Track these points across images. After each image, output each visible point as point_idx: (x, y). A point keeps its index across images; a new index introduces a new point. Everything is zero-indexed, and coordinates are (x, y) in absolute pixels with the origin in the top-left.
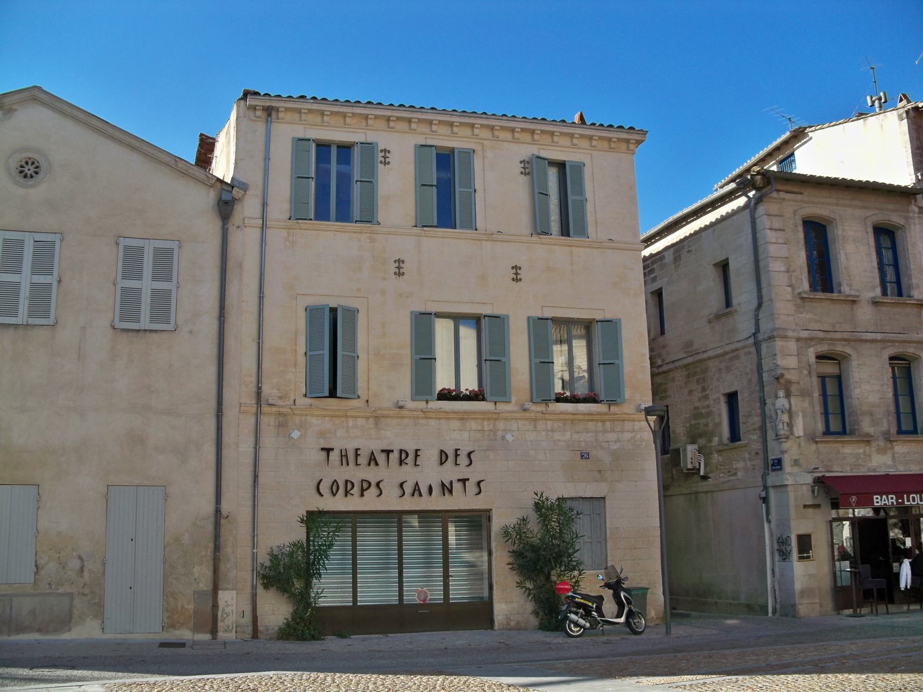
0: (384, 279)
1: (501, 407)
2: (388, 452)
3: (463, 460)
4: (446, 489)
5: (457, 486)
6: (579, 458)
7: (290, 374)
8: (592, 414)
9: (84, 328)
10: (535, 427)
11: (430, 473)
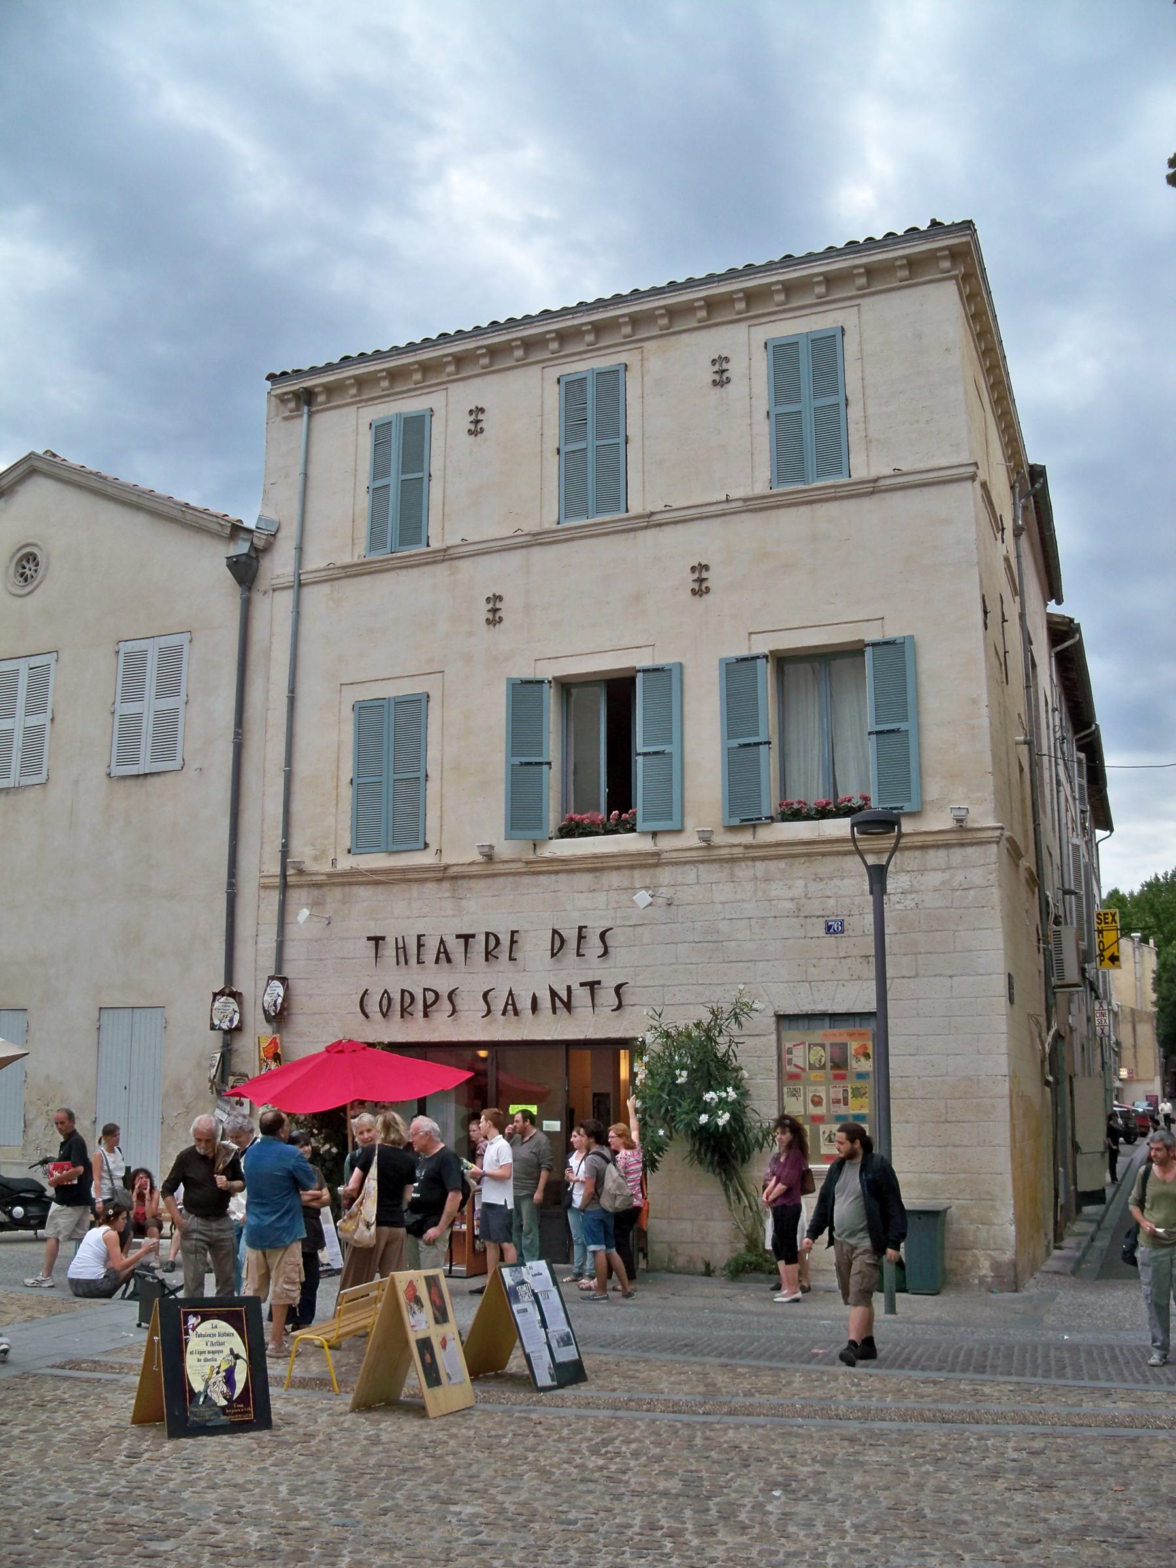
0: (470, 634)
1: (666, 843)
2: (467, 938)
3: (594, 946)
4: (563, 1003)
5: (581, 996)
6: (822, 932)
7: (326, 833)
8: (808, 855)
9: (77, 782)
10: (732, 874)
11: (536, 974)
